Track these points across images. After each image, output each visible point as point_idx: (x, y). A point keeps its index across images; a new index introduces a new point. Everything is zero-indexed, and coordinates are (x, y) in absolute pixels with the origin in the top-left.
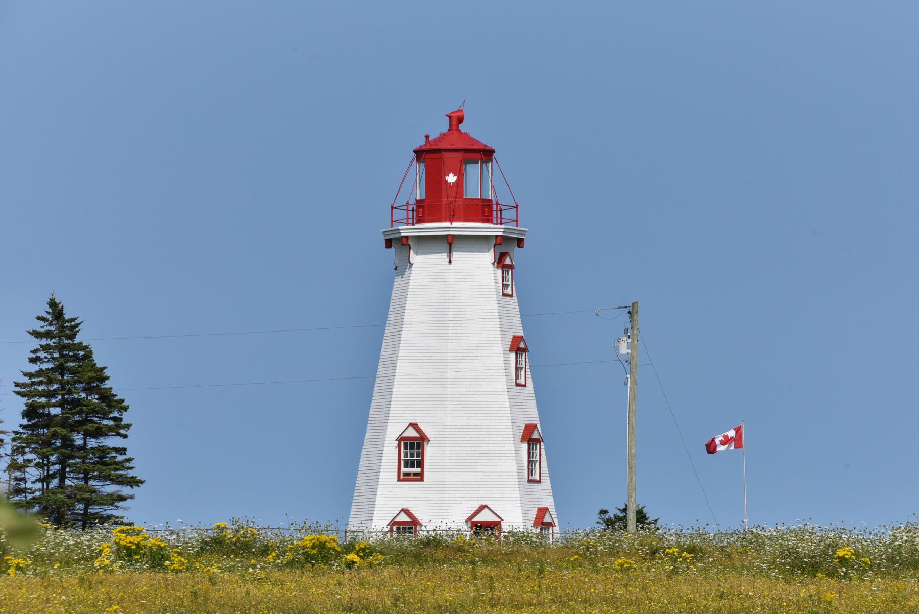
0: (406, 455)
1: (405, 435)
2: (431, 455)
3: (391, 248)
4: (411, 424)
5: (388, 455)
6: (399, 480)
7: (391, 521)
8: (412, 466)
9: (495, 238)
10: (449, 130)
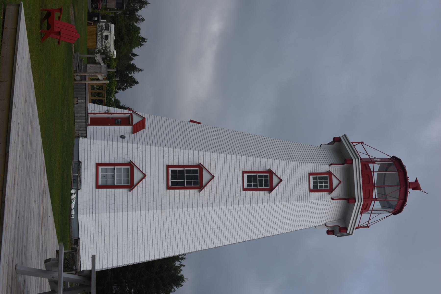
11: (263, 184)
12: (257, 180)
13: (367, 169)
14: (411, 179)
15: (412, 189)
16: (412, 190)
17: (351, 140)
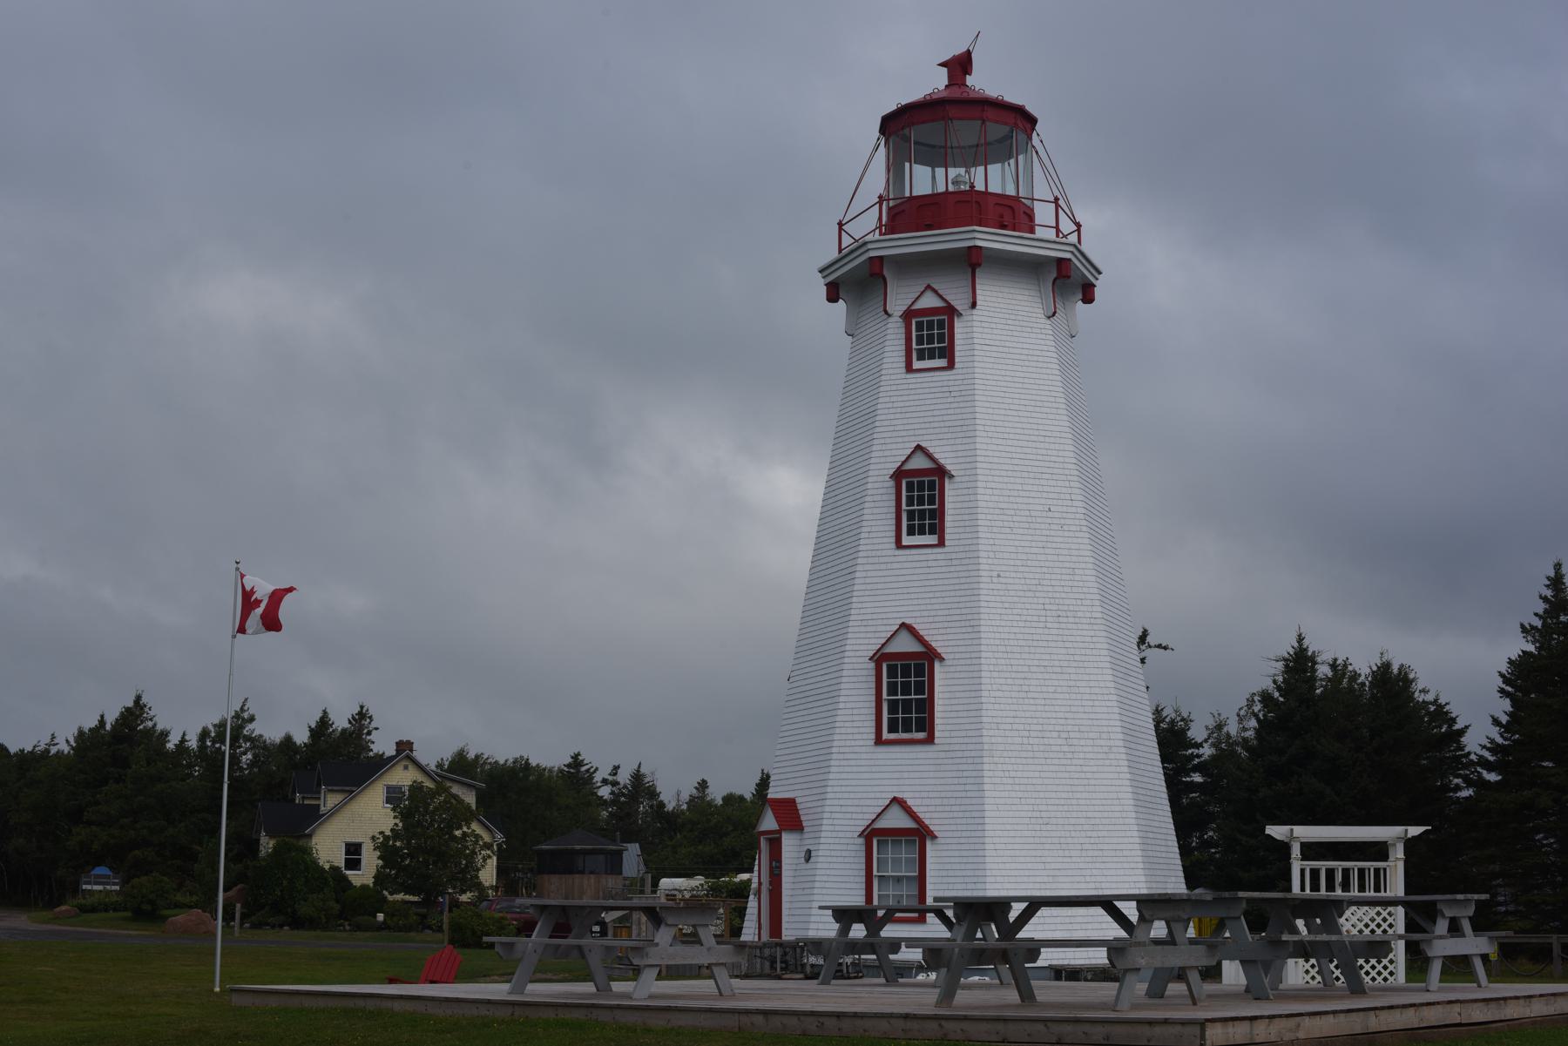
0: (910, 502)
1: (890, 649)
2: (937, 867)
3: (837, 301)
4: (895, 800)
5: (848, 705)
6: (879, 741)
7: (868, 826)
8: (932, 357)
9: (1055, 264)
10: (946, 86)
11: (901, 682)
12: (919, 510)
14: (937, 81)
16: (970, 75)
17: (835, 255)
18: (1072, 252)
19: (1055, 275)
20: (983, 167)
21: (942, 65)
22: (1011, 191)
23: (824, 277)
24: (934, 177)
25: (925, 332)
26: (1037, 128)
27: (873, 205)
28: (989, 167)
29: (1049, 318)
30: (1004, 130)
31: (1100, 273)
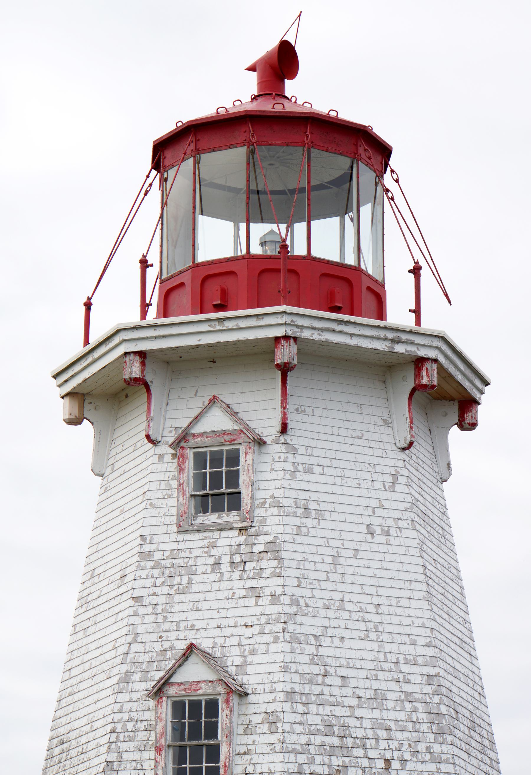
13: (182, 285)
15: (286, 81)
17: (79, 349)
18: (439, 349)
19: (413, 385)
20: (305, 224)
21: (252, 69)
22: (350, 260)
23: (60, 386)
24: (237, 235)
25: (224, 469)
26: (391, 162)
27: (148, 251)
28: (312, 222)
29: (404, 449)
30: (344, 162)
31: (487, 384)
